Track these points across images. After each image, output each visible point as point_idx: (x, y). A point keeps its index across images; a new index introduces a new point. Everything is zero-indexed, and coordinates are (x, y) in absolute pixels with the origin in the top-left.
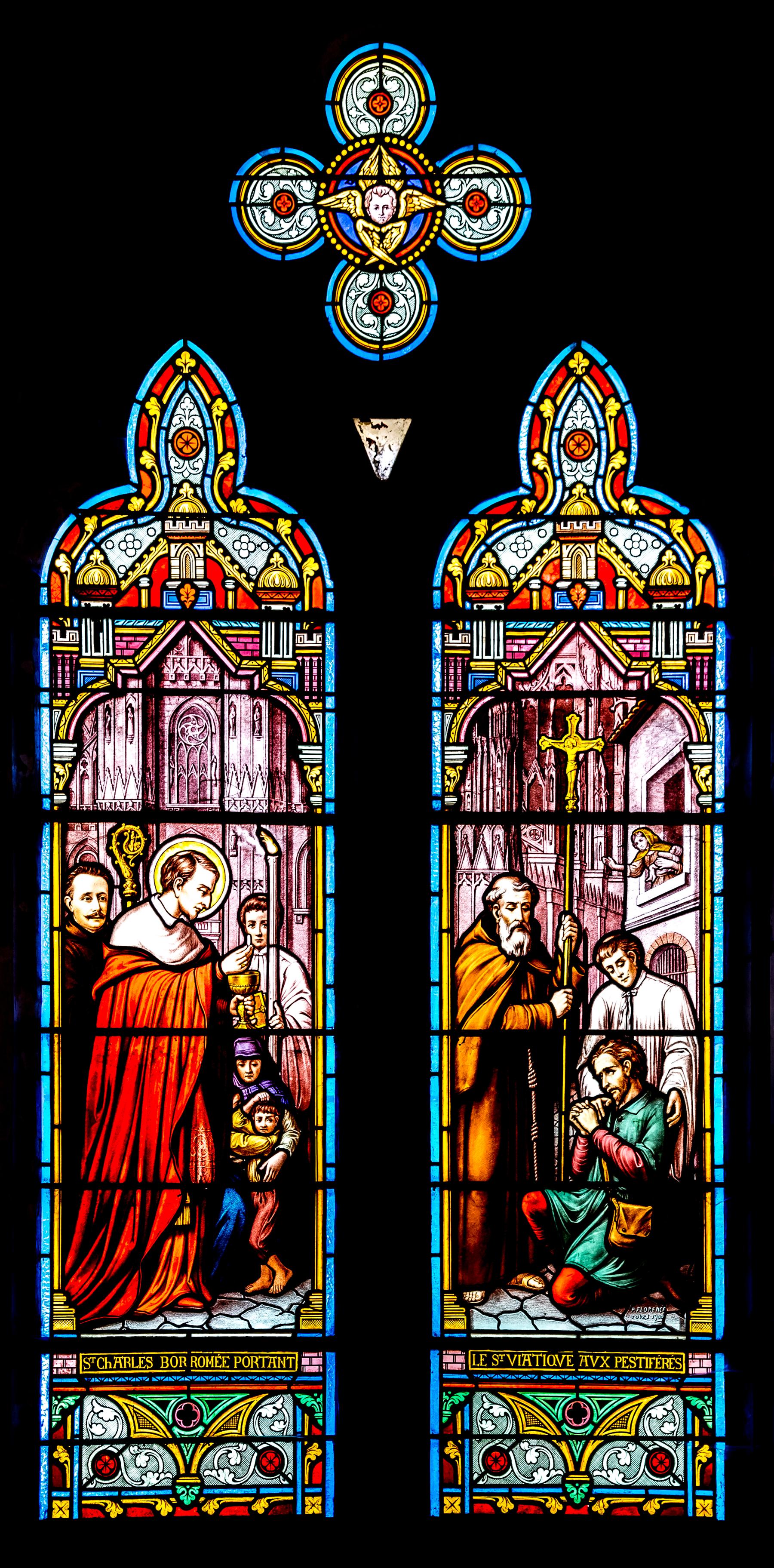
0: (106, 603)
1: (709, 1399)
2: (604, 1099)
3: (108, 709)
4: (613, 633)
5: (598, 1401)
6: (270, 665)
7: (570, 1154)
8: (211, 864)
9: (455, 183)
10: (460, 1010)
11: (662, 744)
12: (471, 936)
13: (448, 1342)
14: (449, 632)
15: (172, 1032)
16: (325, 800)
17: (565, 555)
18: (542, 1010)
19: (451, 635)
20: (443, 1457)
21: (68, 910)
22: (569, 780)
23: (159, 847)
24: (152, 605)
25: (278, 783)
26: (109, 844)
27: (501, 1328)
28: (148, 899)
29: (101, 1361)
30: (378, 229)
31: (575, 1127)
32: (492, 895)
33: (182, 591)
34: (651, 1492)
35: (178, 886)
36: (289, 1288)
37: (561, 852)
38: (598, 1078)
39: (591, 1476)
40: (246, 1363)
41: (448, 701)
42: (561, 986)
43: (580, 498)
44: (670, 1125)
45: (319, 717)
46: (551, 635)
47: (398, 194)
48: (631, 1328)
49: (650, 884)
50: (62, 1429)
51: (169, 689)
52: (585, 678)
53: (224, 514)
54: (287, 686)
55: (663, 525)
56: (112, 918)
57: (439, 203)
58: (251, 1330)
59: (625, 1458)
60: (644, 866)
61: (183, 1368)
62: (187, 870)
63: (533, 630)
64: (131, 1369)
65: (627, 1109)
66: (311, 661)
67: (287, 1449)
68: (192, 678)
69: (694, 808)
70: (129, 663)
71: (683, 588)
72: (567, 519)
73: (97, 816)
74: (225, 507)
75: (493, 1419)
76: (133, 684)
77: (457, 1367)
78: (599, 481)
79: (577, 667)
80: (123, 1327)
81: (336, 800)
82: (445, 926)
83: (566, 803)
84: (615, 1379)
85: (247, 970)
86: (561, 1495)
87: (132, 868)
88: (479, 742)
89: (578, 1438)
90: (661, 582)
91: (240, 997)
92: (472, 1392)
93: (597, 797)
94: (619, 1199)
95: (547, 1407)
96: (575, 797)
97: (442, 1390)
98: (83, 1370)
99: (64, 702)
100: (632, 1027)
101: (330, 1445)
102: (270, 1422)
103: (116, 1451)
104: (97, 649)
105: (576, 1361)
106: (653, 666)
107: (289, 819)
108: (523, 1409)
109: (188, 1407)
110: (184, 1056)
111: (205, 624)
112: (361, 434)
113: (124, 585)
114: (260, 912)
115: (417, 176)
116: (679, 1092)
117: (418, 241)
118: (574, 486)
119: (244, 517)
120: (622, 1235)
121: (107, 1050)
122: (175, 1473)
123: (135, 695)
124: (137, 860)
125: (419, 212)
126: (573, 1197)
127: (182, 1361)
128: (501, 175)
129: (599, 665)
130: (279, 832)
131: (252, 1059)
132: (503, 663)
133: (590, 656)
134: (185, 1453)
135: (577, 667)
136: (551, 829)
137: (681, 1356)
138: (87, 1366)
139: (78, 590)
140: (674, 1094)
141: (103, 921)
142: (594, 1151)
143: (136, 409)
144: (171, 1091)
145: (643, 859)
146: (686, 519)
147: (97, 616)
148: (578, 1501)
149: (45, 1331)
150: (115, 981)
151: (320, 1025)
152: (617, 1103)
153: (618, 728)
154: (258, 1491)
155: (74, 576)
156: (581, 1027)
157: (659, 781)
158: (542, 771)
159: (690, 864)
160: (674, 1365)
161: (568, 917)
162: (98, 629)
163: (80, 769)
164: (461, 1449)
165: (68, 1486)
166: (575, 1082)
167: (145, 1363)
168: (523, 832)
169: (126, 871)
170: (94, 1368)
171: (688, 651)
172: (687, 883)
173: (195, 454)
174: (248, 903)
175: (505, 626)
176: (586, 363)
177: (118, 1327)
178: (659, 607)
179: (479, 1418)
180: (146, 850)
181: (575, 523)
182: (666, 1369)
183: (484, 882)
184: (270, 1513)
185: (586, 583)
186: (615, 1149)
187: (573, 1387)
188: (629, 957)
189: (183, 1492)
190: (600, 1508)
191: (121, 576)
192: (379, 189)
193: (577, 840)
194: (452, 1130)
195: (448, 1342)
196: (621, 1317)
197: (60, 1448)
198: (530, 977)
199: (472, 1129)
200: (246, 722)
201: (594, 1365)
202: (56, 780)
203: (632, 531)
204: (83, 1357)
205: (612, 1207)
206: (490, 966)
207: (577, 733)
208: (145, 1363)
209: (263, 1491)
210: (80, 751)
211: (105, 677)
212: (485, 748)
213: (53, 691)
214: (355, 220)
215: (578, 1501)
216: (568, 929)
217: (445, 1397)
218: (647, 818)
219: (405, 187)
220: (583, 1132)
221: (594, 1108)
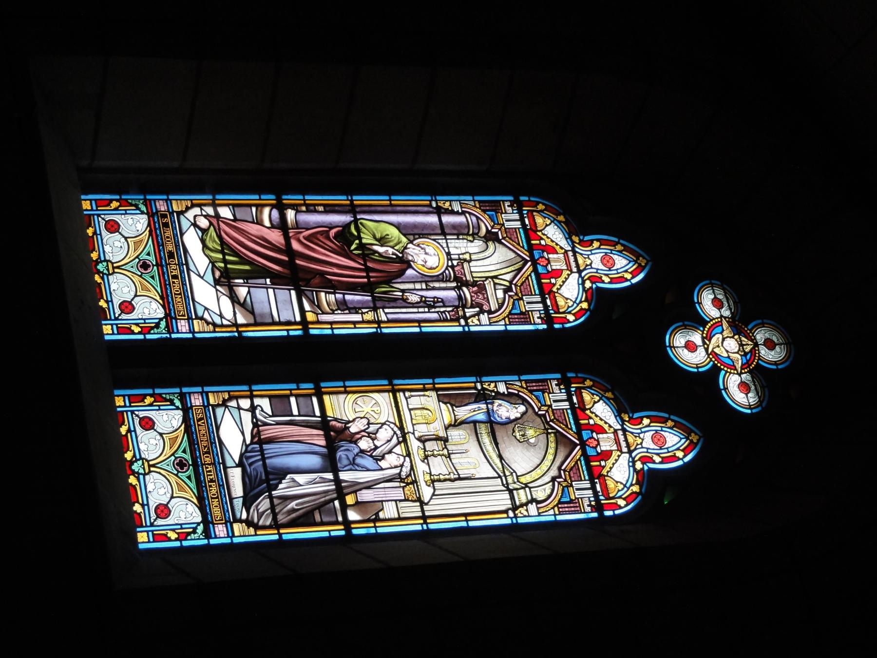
5: (154, 275)
6: (570, 486)
17: (559, 255)
24: (582, 426)
34: (146, 507)
53: (633, 459)
58: (182, 234)
63: (569, 418)
66: (577, 507)
78: (645, 450)
84: (167, 283)
90: (608, 482)
95: (182, 449)
98: (195, 409)
109: (149, 266)
111: (580, 452)
113: (588, 412)
122: (149, 459)
128: (759, 397)
155: (584, 388)
165: (99, 208)
171: (580, 499)
173: (605, 265)
178: (597, 483)
184: (135, 515)
189: (138, 464)
190: (132, 480)
191: (543, 232)
201: (199, 423)
217: (176, 396)
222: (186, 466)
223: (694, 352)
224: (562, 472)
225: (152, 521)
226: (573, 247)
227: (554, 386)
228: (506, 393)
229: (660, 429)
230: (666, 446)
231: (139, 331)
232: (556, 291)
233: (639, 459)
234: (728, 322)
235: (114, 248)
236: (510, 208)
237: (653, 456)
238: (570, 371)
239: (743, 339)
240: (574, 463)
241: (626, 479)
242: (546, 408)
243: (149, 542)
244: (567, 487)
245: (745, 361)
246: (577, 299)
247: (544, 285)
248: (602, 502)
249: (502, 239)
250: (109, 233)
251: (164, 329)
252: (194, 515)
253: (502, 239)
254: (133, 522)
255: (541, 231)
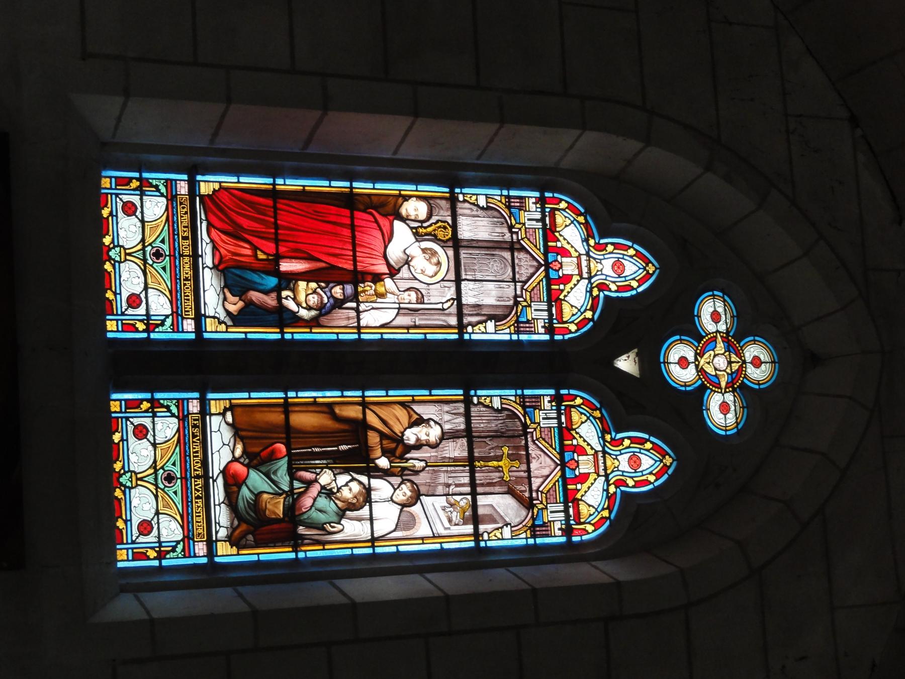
0: (548, 225)
1: (182, 555)
2: (336, 488)
3: (503, 224)
4: (557, 483)
7: (306, 470)
8: (436, 274)
9: (732, 398)
10: (375, 407)
11: (510, 511)
12: (412, 413)
13: (204, 403)
14: (551, 398)
15: (354, 251)
16: (470, 334)
18: (378, 452)
19: (550, 399)
20: (141, 401)
21: (409, 199)
22: (489, 463)
23: (442, 247)
25: (476, 309)
26: (442, 222)
27: (213, 433)
28: (417, 241)
29: (185, 207)
30: (711, 361)
31: (321, 472)
32: (432, 423)
33: (557, 263)
35: (425, 257)
36: (228, 313)
37: (455, 460)
38: (346, 485)
39: (135, 487)
40: (187, 288)
41: (520, 398)
42: (391, 462)
43: (613, 463)
44: (325, 526)
45: (508, 331)
46: (554, 451)
47: (725, 371)
48: (217, 507)
49: (444, 509)
50: (148, 185)
51: (514, 255)
52: (536, 470)
53: (592, 284)
54: (520, 314)
55: (605, 507)
56: (407, 222)
57: (723, 391)
58: (204, 291)
59: (146, 507)
60: (452, 505)
61: (183, 253)
62: (432, 261)
63: (555, 442)
64: (181, 224)
65: (332, 501)
66: (532, 327)
67: (142, 310)
68: (520, 266)
69: (481, 530)
70: (524, 236)
71: (580, 518)
72: (604, 457)
73: (454, 216)
74: (594, 285)
75: (164, 429)
76: (515, 236)
77: (191, 408)
78: (621, 473)
79: (541, 465)
80: (204, 220)
81: (470, 340)
82: (416, 398)
83: (479, 462)
84: (189, 500)
85: (387, 292)
86: (124, 470)
87: (431, 232)
88: (503, 415)
89: (156, 479)
90: (581, 507)
91: (373, 288)
92: (177, 417)
93: (483, 478)
94: (285, 498)
96: (481, 467)
97: (178, 400)
98: (180, 197)
99: (504, 202)
100: (374, 502)
101: (145, 335)
102: (156, 301)
103: (137, 214)
104: (529, 220)
105: (198, 477)
106: (544, 505)
107: (460, 315)
108: (170, 447)
109: (161, 255)
110: (343, 257)
111: (559, 474)
112: (631, 352)
113: (557, 234)
114: (416, 299)
115: (733, 379)
116: (342, 530)
117: (709, 380)
118: (618, 460)
119: (591, 295)
120: (266, 501)
121: (343, 216)
123: (510, 238)
124: (435, 236)
125: (719, 380)
126: (284, 473)
127: (186, 252)
128: (737, 419)
129: (542, 477)
130: (454, 310)
131: (344, 294)
132: (539, 427)
133: (546, 472)
134: (138, 253)
135: (541, 465)
136: (465, 454)
137: (204, 538)
138: (182, 200)
139: (553, 211)
140: (340, 527)
141: (405, 217)
142: (309, 483)
143: (630, 244)
144: (326, 250)
145: (456, 504)
146: (609, 518)
147: (542, 220)
148: (121, 480)
149: (199, 178)
150: (376, 222)
151: (362, 331)
152: (334, 496)
153: (515, 488)
154: (118, 294)
155: (558, 210)
156: (372, 474)
157: (493, 511)
158: (492, 448)
159: (455, 530)
160: (199, 534)
161: (425, 465)
162: (537, 220)
163: (475, 208)
164: (146, 411)
165: (128, 411)
166: (346, 471)
167: (185, 232)
168: (463, 439)
169: (429, 229)
170: (181, 204)
172: (446, 529)
173: (615, 271)
174: (419, 293)
175: (555, 427)
176: (668, 464)
177: (203, 217)
178: (570, 507)
179: (163, 421)
180: (440, 240)
181: (603, 462)
182: (197, 529)
183: (438, 419)
185: (577, 469)
186: (311, 495)
187: (183, 476)
188: (408, 499)
189: (116, 251)
191: (577, 430)
192: (726, 362)
193: (462, 468)
194: (315, 403)
195: (204, 403)
196: (223, 502)
197: (138, 183)
198: (393, 445)
199: (316, 415)
200: (502, 294)
201: (196, 487)
202: (469, 196)
203: (601, 490)
204: (187, 198)
205: (280, 495)
206: (398, 423)
207: (511, 466)
208: (185, 232)
209: (118, 296)
210: (482, 208)
211: (516, 223)
212: (500, 418)
213: (508, 197)
214: (713, 350)
215: (121, 480)
216: (419, 465)
217: (162, 181)
218: (474, 506)
219: (728, 374)
220: (318, 477)
221: (331, 483)
222: (162, 257)
223: (683, 369)
224: (524, 291)
225: (123, 310)
226: (604, 446)
227: (531, 205)
228: (485, 207)
229: (638, 450)
230: (640, 469)
231: (143, 329)
232: (563, 298)
233: (596, 286)
234: (722, 337)
235: (142, 503)
236: (534, 205)
237: (627, 480)
238: (549, 191)
239: (733, 356)
240: (536, 284)
241: (580, 305)
242: (520, 226)
243: (118, 331)
244: (542, 509)
245: (730, 380)
246: (582, 307)
247: (547, 199)
248: (555, 325)
249: (521, 240)
250: (137, 440)
251: (170, 327)
252: (175, 532)
253: (521, 240)
254: (106, 308)
255: (559, 232)
